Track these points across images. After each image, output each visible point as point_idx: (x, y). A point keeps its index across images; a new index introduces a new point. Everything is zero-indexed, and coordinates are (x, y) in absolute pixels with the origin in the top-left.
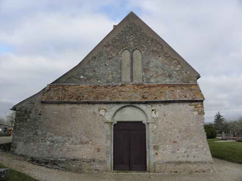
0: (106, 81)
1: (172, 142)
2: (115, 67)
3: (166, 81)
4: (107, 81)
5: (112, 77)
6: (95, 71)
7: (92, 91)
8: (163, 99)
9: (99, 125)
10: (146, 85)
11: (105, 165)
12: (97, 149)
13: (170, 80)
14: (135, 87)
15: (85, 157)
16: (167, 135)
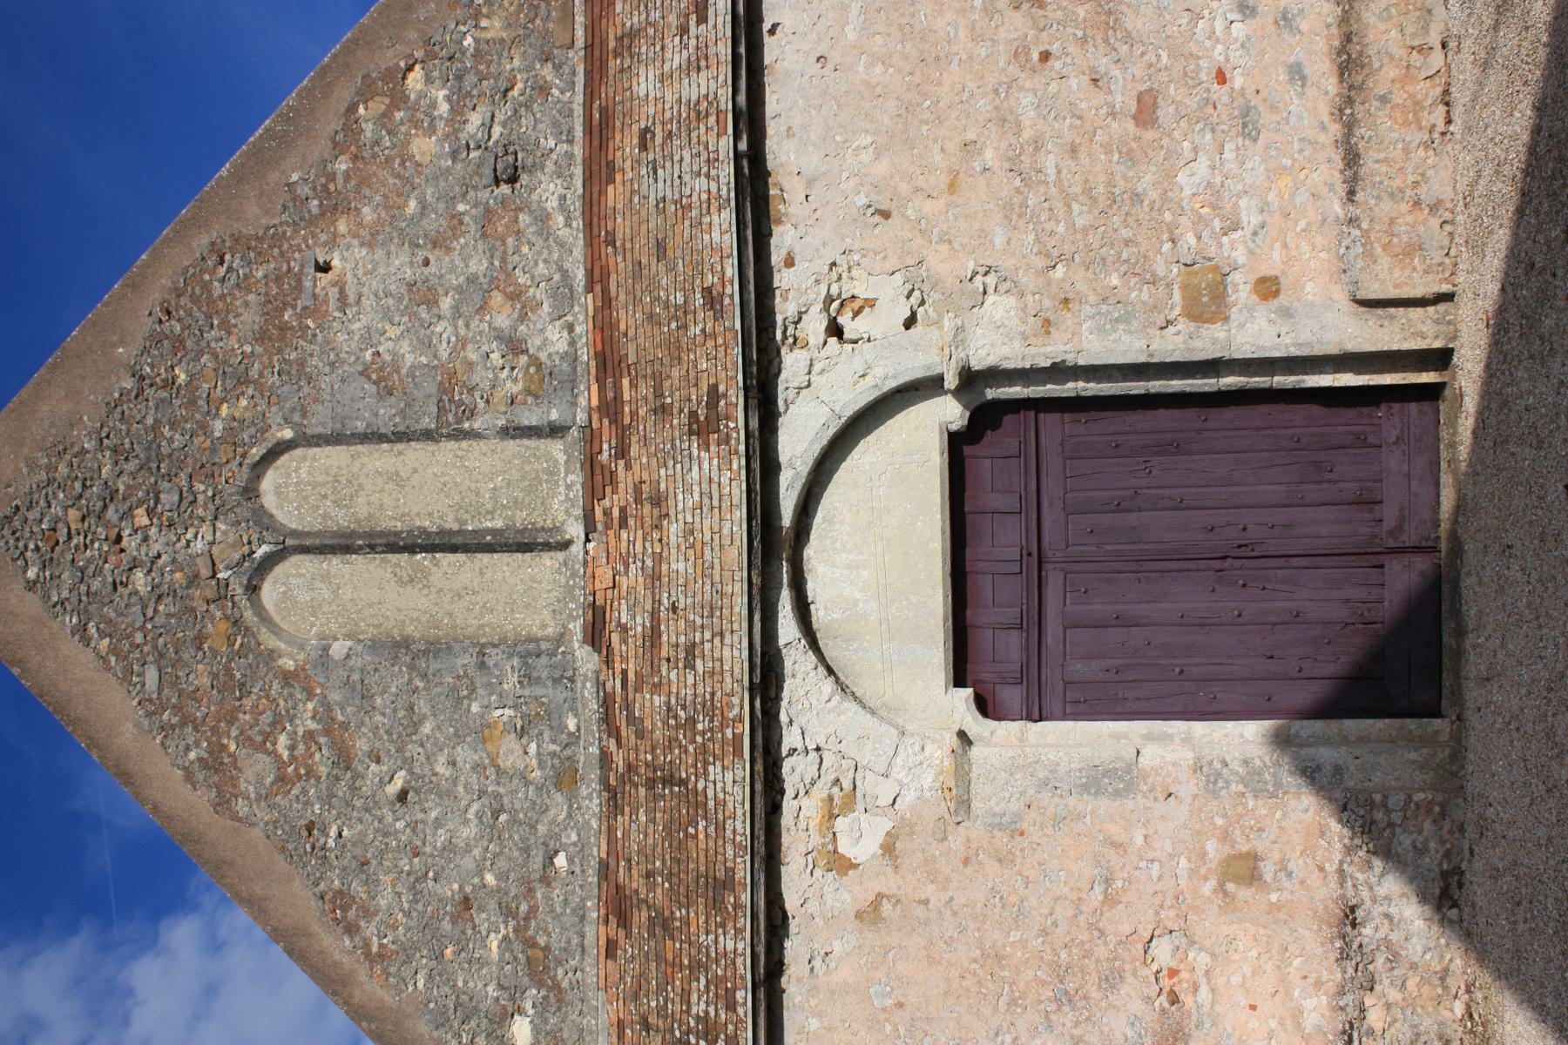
0: (559, 797)
1: (1149, 135)
2: (422, 706)
3: (552, 204)
4: (558, 786)
5: (522, 733)
6: (466, 903)
7: (652, 935)
8: (722, 228)
9: (992, 867)
10: (595, 402)
11: (1396, 800)
12: (1230, 887)
13: (550, 166)
14: (616, 513)
15: (1310, 1003)
16: (1078, 189)
